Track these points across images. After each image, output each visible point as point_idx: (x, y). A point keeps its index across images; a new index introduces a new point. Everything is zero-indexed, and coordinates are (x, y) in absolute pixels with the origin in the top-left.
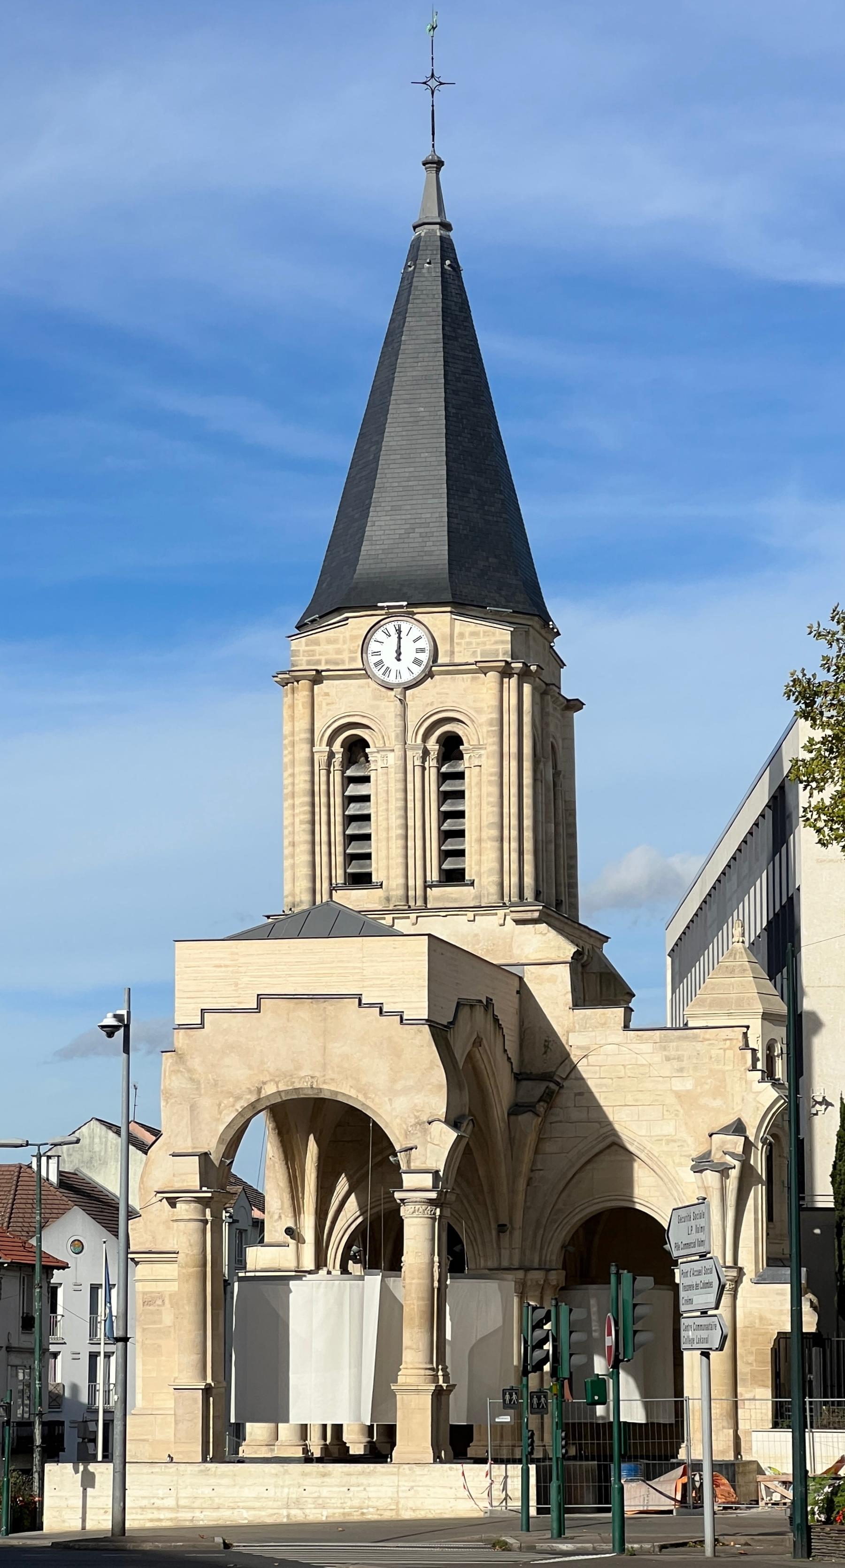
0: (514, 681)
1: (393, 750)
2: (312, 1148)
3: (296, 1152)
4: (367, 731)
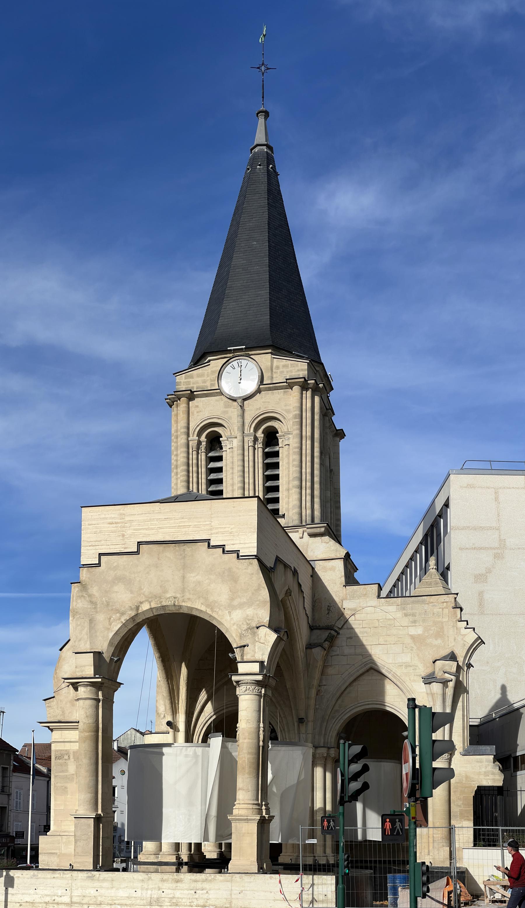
0: (309, 393)
1: (236, 437)
2: (184, 670)
3: (174, 674)
4: (220, 428)
